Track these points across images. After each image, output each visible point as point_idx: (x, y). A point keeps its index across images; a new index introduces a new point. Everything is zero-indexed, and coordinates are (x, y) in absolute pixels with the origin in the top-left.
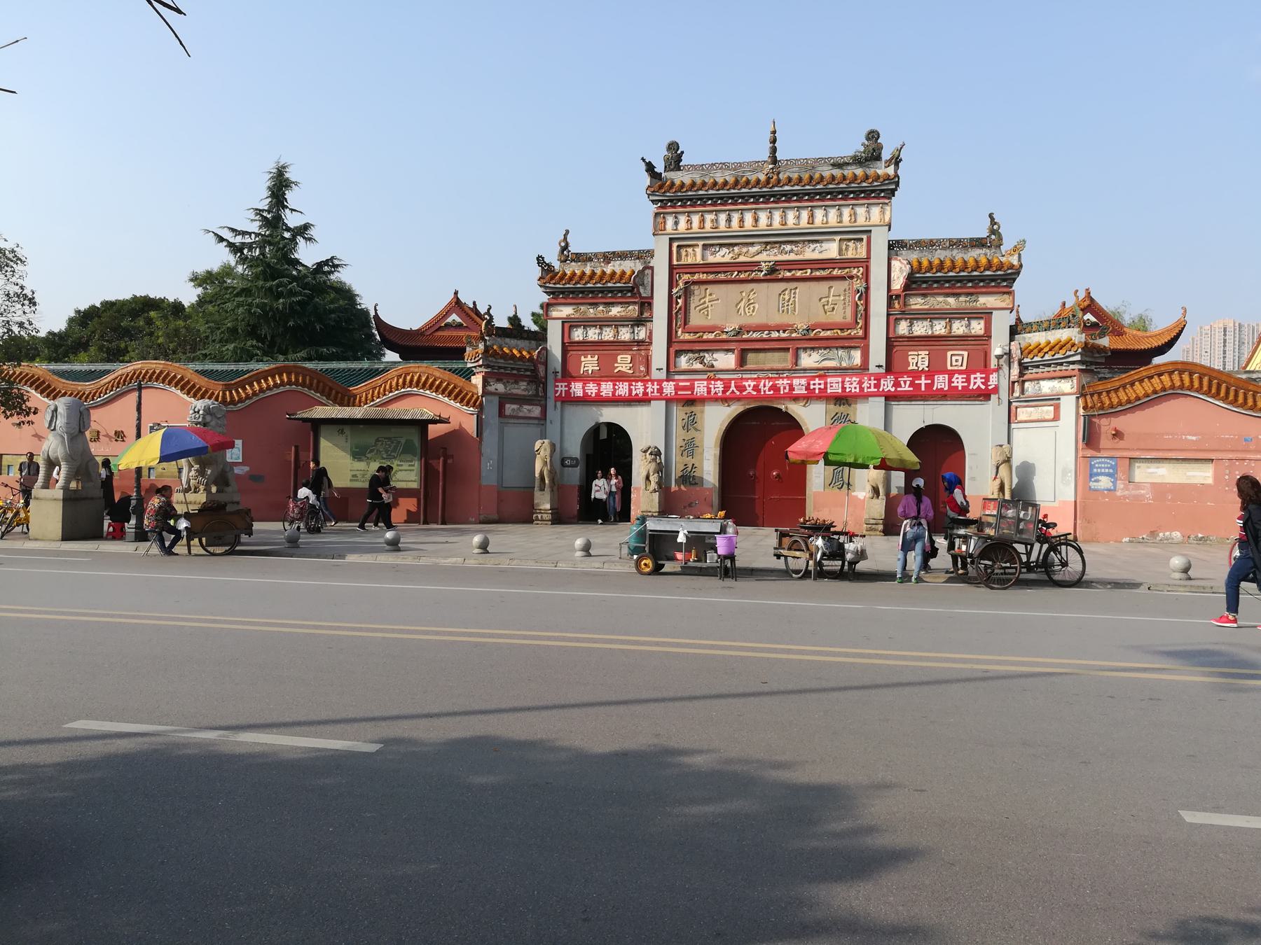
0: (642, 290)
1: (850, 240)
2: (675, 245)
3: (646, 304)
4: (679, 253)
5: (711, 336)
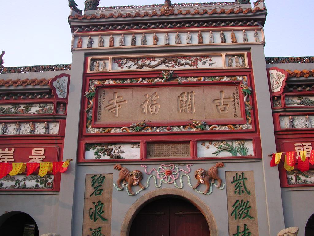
0: (58, 92)
1: (234, 56)
2: (90, 58)
3: (63, 104)
4: (92, 65)
5: (119, 131)
